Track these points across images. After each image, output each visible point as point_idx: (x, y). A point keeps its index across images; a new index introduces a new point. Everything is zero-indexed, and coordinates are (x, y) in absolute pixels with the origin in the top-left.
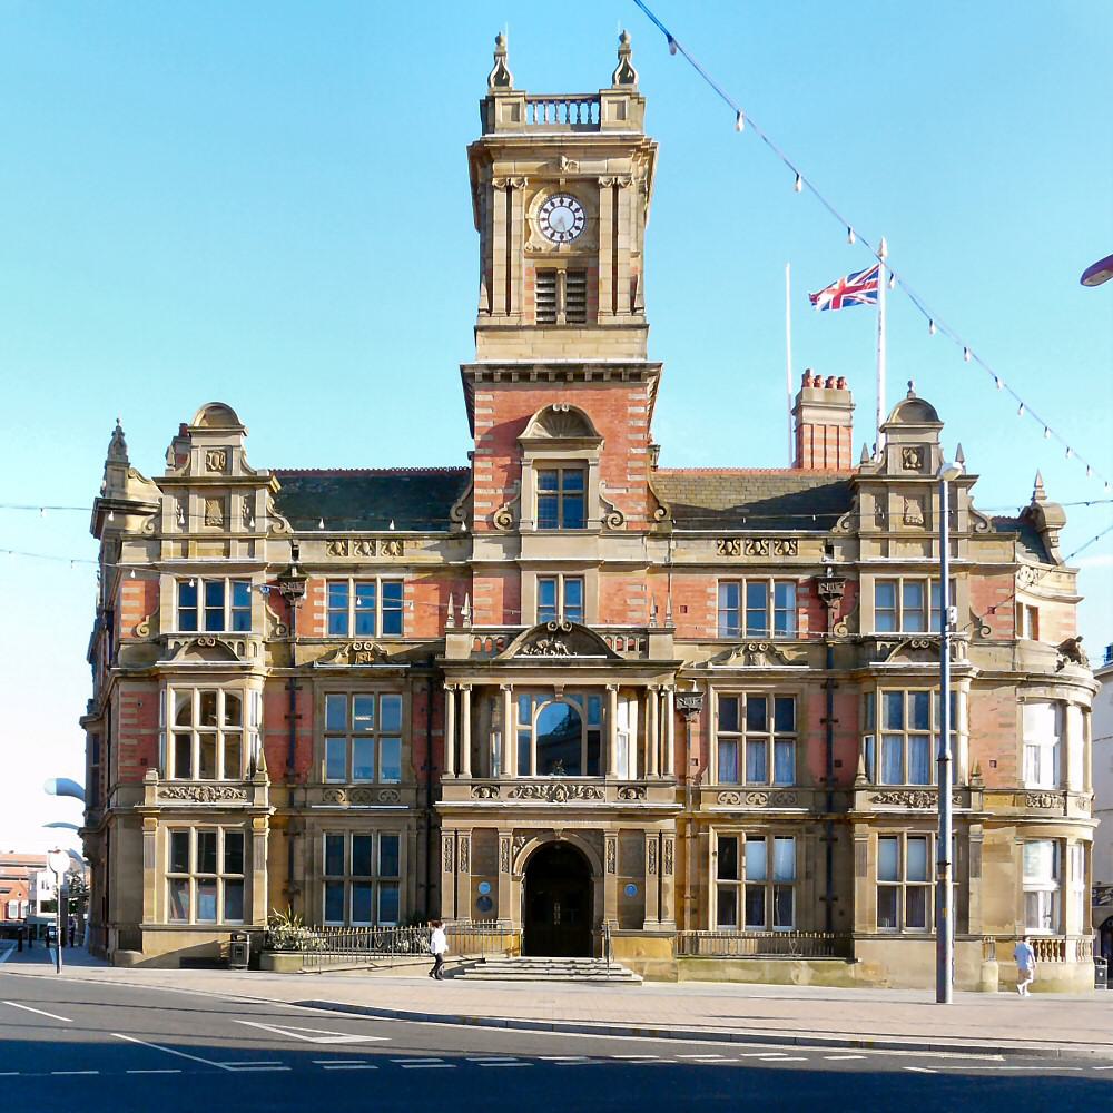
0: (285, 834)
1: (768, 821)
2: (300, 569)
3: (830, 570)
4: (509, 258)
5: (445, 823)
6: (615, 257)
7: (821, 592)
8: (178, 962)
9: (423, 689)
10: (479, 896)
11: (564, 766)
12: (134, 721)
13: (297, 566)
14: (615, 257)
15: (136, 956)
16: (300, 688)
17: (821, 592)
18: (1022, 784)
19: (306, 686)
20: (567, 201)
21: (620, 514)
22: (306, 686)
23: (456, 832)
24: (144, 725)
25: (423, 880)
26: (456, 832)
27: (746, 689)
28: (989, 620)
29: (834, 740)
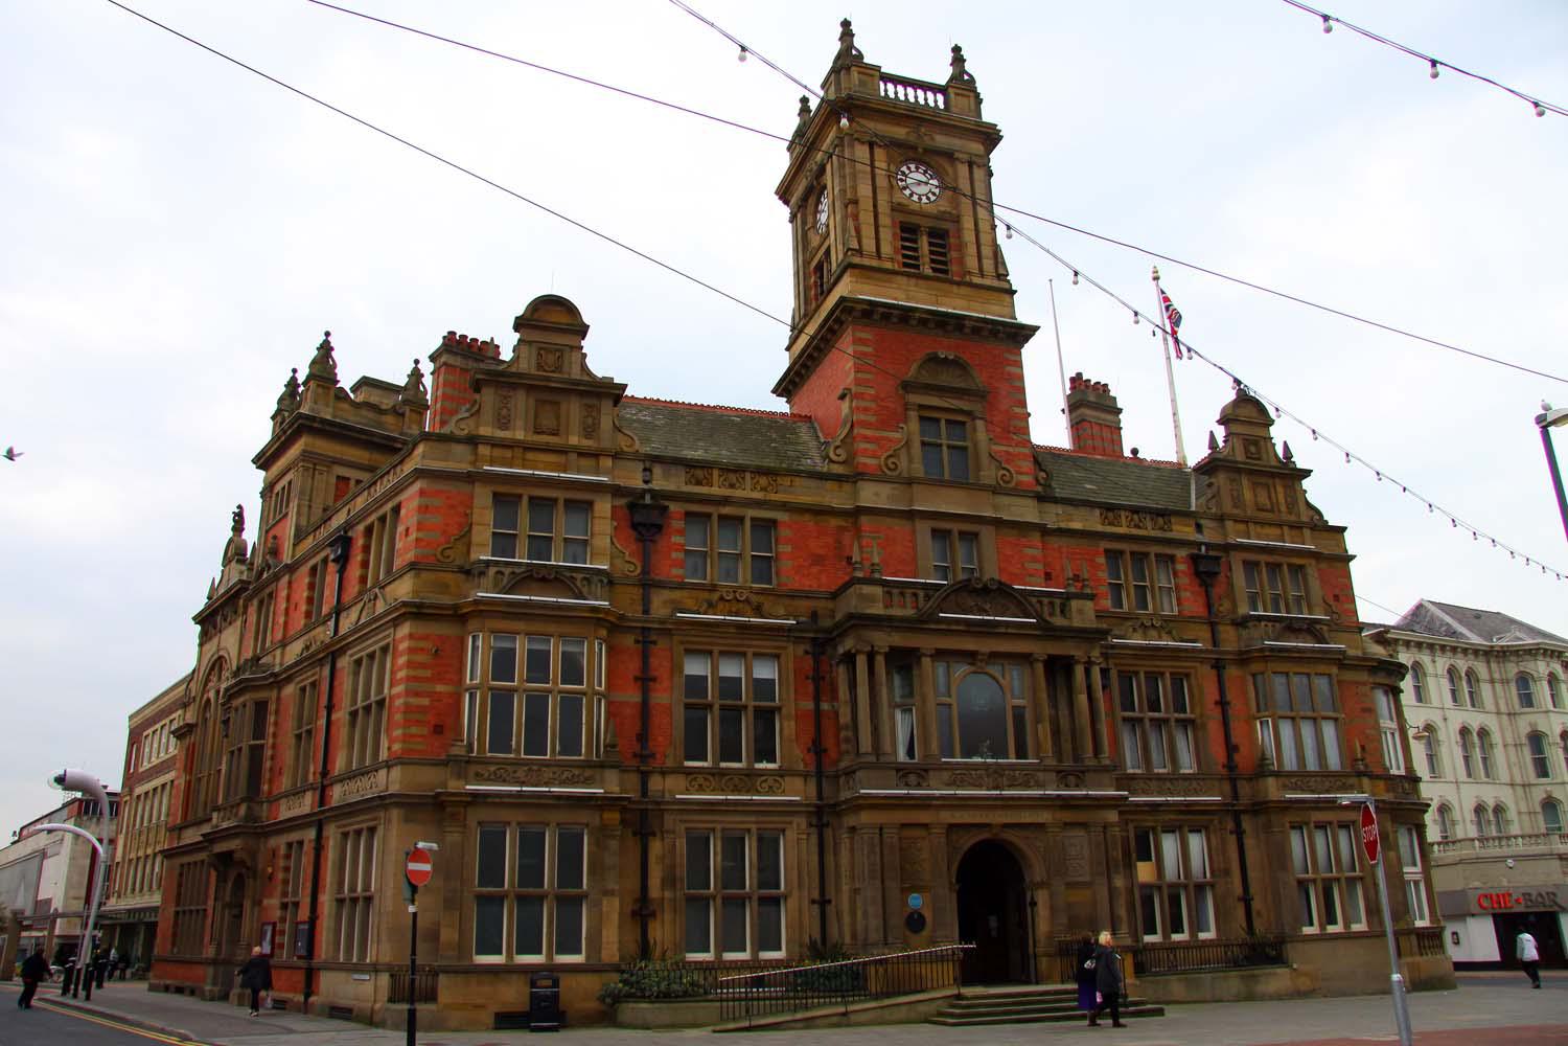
0: (635, 834)
1: (1181, 812)
2: (655, 494)
3: (1203, 548)
4: (875, 206)
5: (1420, 870)
6: (976, 224)
8: (490, 1020)
9: (807, 652)
10: (909, 911)
11: (990, 749)
12: (428, 673)
13: (650, 491)
14: (976, 224)
15: (178, 718)
16: (654, 643)
17: (1202, 569)
18: (1387, 770)
19: (662, 643)
21: (1008, 471)
22: (662, 643)
23: (881, 829)
24: (438, 678)
25: (816, 895)
26: (881, 829)
27: (1144, 666)
28: (1336, 607)
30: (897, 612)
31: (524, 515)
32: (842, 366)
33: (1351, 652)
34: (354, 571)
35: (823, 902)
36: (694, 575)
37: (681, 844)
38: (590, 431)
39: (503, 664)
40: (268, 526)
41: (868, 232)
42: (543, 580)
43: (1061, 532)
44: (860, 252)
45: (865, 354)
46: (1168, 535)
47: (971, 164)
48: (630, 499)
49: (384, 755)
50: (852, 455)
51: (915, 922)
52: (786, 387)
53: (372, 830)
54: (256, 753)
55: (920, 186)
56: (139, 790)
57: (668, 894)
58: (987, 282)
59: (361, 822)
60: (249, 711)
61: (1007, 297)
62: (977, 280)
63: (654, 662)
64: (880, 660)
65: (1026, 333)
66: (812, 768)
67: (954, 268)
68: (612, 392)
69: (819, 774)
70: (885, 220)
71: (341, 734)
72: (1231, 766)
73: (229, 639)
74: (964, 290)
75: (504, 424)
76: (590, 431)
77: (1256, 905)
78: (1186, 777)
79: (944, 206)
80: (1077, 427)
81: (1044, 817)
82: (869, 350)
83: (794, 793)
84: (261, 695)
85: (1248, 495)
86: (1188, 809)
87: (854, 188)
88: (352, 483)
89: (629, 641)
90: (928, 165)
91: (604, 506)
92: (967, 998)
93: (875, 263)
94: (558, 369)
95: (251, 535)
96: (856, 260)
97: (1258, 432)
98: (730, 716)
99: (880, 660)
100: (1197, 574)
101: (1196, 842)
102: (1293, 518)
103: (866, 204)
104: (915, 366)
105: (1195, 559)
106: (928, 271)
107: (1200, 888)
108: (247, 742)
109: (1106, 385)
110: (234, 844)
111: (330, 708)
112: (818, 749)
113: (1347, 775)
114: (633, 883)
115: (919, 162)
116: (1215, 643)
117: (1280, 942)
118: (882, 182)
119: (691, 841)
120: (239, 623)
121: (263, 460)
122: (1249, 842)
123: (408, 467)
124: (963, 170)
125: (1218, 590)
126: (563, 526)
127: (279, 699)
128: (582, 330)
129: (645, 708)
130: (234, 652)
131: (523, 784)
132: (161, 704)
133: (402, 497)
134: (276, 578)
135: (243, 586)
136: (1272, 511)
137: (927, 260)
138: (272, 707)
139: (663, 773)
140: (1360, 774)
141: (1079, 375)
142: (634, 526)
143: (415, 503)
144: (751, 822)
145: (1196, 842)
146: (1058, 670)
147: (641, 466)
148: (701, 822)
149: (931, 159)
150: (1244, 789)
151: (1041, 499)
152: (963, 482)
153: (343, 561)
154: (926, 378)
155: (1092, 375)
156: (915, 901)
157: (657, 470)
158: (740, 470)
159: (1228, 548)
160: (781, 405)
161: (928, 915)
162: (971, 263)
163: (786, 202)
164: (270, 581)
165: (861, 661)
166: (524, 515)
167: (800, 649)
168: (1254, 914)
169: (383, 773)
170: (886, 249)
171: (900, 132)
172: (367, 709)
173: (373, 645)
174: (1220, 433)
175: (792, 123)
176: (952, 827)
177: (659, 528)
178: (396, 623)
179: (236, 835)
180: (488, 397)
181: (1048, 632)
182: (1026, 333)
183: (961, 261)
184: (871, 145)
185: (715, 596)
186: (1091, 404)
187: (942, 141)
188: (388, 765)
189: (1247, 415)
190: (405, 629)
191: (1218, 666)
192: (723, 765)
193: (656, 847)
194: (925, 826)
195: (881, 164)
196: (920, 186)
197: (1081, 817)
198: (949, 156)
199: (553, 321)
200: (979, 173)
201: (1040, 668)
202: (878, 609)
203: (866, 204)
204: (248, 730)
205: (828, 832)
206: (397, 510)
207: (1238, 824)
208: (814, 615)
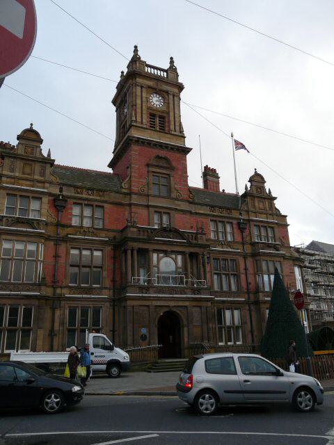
20: (158, 96)
29: (248, 276)
30: (141, 237)
33: (287, 254)
37: (67, 312)
42: (22, 223)
43: (196, 213)
44: (136, 121)
47: (174, 96)
51: (144, 338)
52: (111, 165)
58: (176, 133)
61: (183, 139)
64: (135, 252)
65: (188, 150)
68: (49, 162)
70: (144, 112)
74: (169, 136)
76: (43, 174)
77: (255, 333)
80: (205, 182)
81: (187, 304)
83: (105, 295)
85: (256, 204)
92: (157, 363)
93: (141, 126)
94: (32, 153)
96: (135, 124)
99: (135, 252)
100: (239, 228)
102: (270, 212)
105: (239, 224)
107: (237, 328)
115: (156, 93)
122: (253, 313)
124: (171, 97)
126: (35, 205)
128: (41, 141)
131: (11, 291)
141: (207, 166)
144: (91, 304)
145: (236, 313)
148: (73, 304)
149: (162, 93)
151: (190, 203)
155: (211, 166)
156: (144, 331)
158: (92, 190)
160: (110, 171)
161: (148, 336)
162: (172, 127)
163: (115, 105)
165: (129, 252)
170: (144, 121)
174: (249, 185)
175: (119, 79)
181: (190, 245)
182: (188, 150)
186: (210, 174)
187: (165, 87)
189: (257, 180)
191: (245, 258)
193: (58, 313)
196: (156, 101)
198: (167, 92)
199: (31, 137)
207: (250, 308)
208: (115, 237)
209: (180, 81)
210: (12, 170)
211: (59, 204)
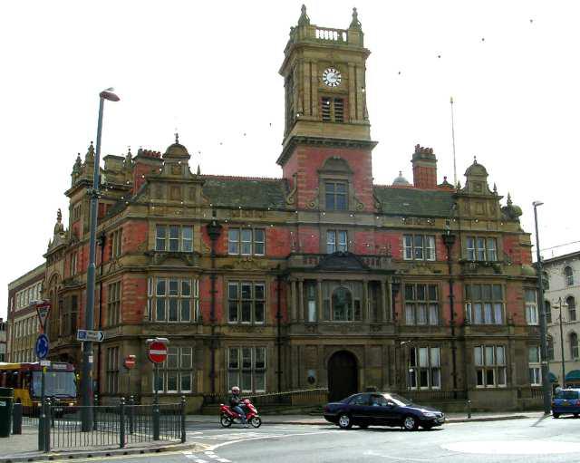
4: (311, 91)
7: (446, 240)
12: (133, 292)
19: (220, 278)
22: (220, 278)
30: (308, 265)
31: (168, 233)
32: (295, 156)
34: (107, 250)
35: (279, 373)
36: (233, 251)
38: (192, 198)
39: (161, 289)
40: (73, 221)
41: (307, 104)
43: (383, 228)
45: (303, 158)
46: (434, 227)
47: (355, 67)
48: (206, 224)
49: (120, 321)
50: (297, 200)
51: (311, 380)
53: (117, 348)
54: (74, 315)
55: (331, 78)
56: (16, 320)
57: (222, 369)
58: (358, 122)
59: (113, 345)
60: (70, 299)
62: (354, 121)
63: (216, 286)
64: (301, 285)
66: (276, 324)
67: (345, 116)
69: (279, 326)
71: (106, 313)
72: (452, 322)
73: (59, 266)
75: (159, 197)
78: (432, 327)
79: (344, 88)
81: (362, 342)
82: (304, 156)
84: (75, 293)
86: (431, 339)
87: (303, 84)
88: (105, 206)
89: (207, 278)
90: (337, 69)
91: (197, 227)
93: (309, 118)
95: (66, 224)
97: (481, 179)
98: (246, 309)
101: (500, 352)
103: (307, 91)
104: (323, 164)
105: (444, 237)
106: (333, 119)
108: (70, 312)
109: (431, 149)
110: (67, 351)
111: (101, 302)
112: (278, 316)
113: (503, 326)
114: (208, 366)
115: (332, 67)
116: (450, 272)
117: (466, 391)
118: (314, 80)
119: (231, 351)
120: (62, 261)
121: (69, 194)
122: (458, 352)
123: (125, 214)
124: (352, 70)
125: (455, 248)
127: (81, 295)
129: (213, 304)
130: (61, 273)
132: (22, 281)
133: (123, 225)
134: (77, 246)
135: (64, 247)
136: (483, 214)
137: (333, 110)
138: (79, 298)
139: (220, 326)
140: (509, 325)
141: (418, 145)
142: (209, 235)
143: (128, 229)
145: (500, 352)
146: (375, 285)
147: (212, 210)
150: (457, 331)
152: (343, 208)
153: (103, 245)
154: (330, 168)
155: (425, 145)
156: (311, 373)
157: (218, 211)
158: (249, 209)
159: (460, 232)
161: (315, 377)
162: (353, 114)
164: (75, 247)
166: (168, 233)
167: (273, 279)
168: (457, 380)
169: (120, 327)
170: (314, 110)
171: (322, 55)
172: (114, 304)
173: (115, 280)
176: (326, 346)
177: (219, 235)
178: (123, 273)
179: (67, 348)
180: (153, 187)
183: (349, 112)
184: (310, 63)
185: (241, 260)
187: (342, 57)
188: (122, 325)
190: (126, 276)
191: (451, 282)
192: (243, 323)
193: (218, 353)
194: (316, 346)
195: (314, 74)
196: (331, 78)
197: (379, 342)
198: (346, 64)
200: (358, 71)
201: (366, 286)
202: (301, 265)
203: (307, 91)
204: (70, 307)
205: (282, 347)
206: (121, 229)
209: (365, 46)
210: (159, 197)
211: (213, 231)
